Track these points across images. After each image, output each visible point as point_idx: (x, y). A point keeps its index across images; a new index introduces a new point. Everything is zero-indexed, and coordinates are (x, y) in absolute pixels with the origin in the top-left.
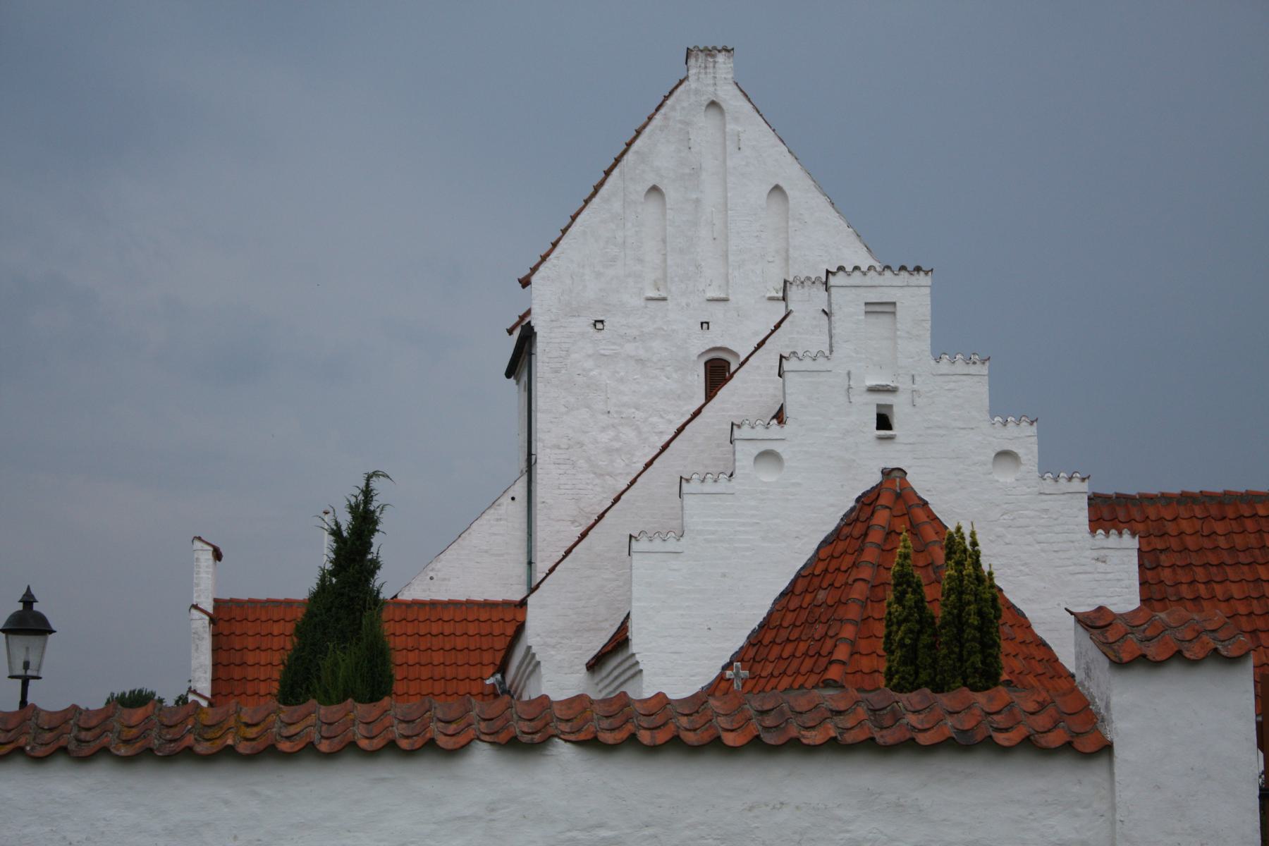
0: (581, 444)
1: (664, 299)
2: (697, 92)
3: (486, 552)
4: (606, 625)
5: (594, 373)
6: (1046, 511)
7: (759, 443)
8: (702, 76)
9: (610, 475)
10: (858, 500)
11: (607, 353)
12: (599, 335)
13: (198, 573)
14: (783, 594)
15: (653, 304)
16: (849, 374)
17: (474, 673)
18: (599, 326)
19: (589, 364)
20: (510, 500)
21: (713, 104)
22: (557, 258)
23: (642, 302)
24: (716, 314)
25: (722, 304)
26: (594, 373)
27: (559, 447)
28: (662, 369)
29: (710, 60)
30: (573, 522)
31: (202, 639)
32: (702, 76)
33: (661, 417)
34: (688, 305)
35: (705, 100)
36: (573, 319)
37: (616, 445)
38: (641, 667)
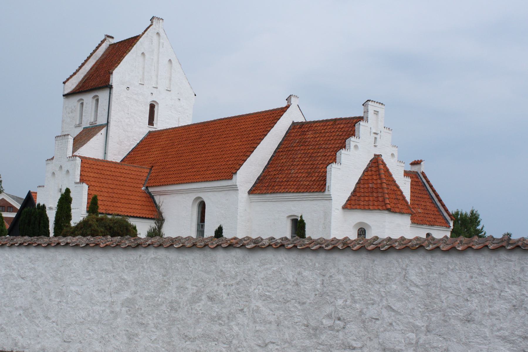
0: (121, 121)
1: (143, 85)
2: (155, 29)
3: (93, 148)
4: (252, 182)
5: (126, 102)
6: (398, 170)
7: (355, 143)
8: (156, 25)
9: (127, 131)
10: (370, 161)
11: (129, 97)
12: (128, 91)
13: (69, 145)
14: (358, 183)
15: (140, 85)
16: (371, 128)
17: (138, 185)
18: (128, 89)
19: (125, 99)
20: (390, 155)
21: (158, 33)
22: (120, 67)
23: (138, 84)
24: (154, 91)
25: (156, 89)
26: (126, 102)
27: (116, 121)
28: (141, 104)
29: (158, 21)
30: (117, 143)
31: (78, 166)
32: (156, 25)
33: (140, 117)
34: (149, 87)
35: (156, 32)
36: (122, 86)
37: (129, 123)
38: (332, 198)
